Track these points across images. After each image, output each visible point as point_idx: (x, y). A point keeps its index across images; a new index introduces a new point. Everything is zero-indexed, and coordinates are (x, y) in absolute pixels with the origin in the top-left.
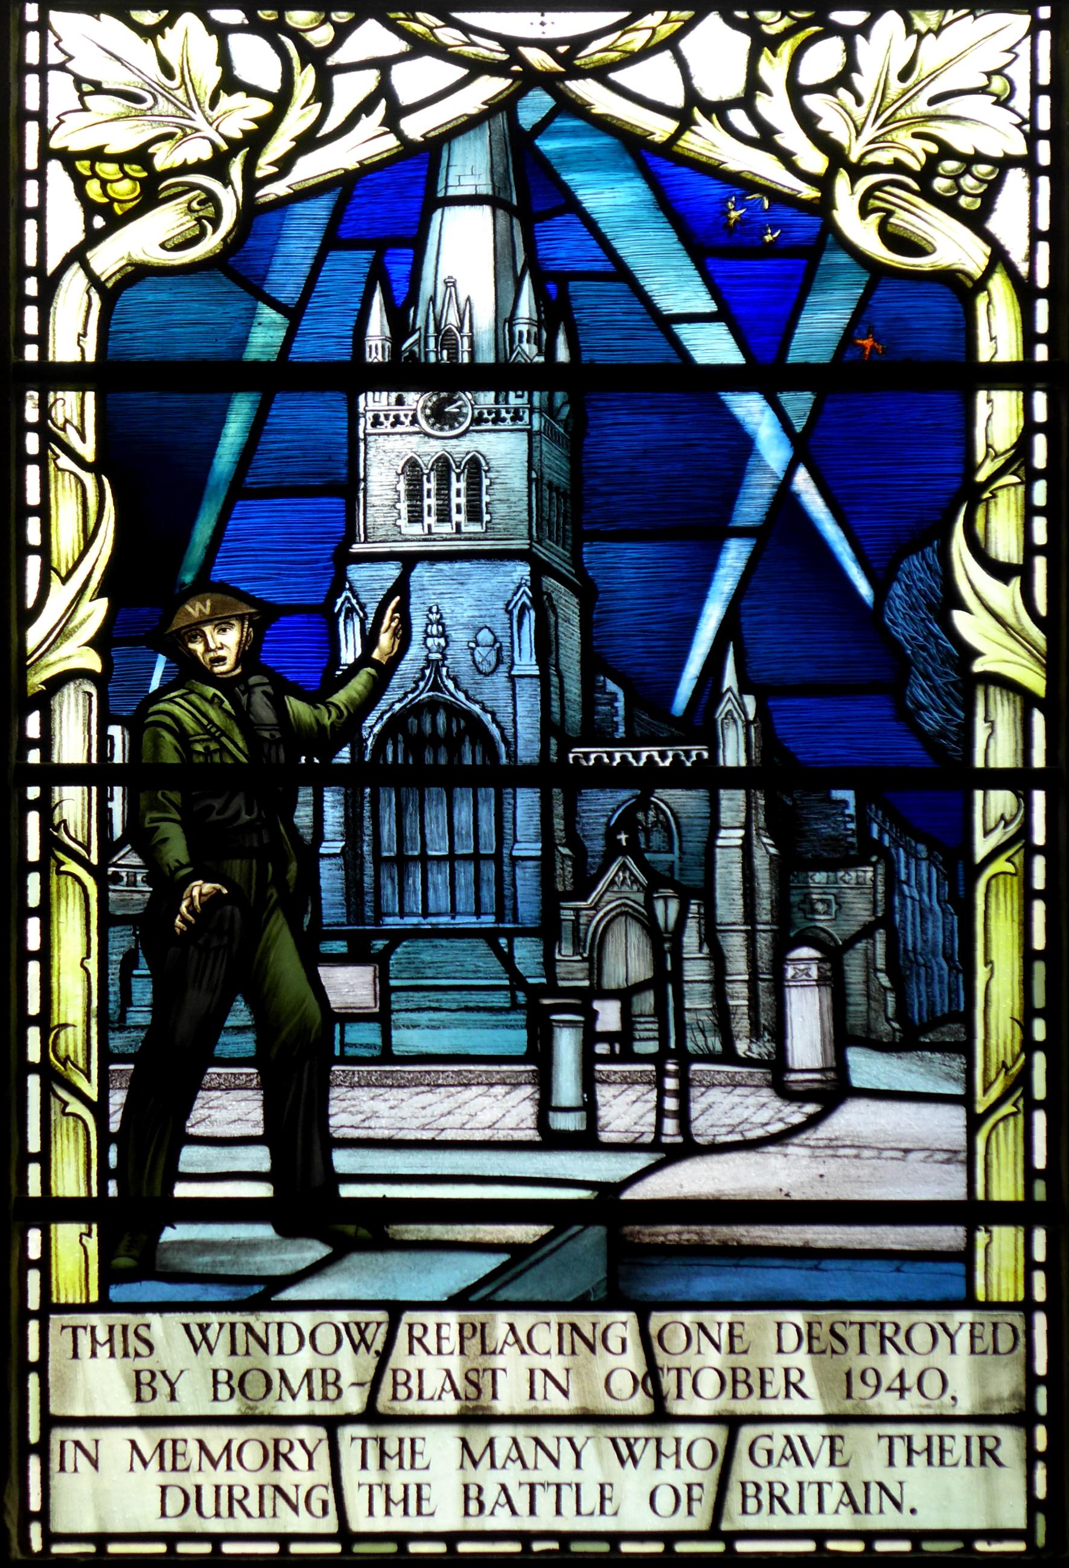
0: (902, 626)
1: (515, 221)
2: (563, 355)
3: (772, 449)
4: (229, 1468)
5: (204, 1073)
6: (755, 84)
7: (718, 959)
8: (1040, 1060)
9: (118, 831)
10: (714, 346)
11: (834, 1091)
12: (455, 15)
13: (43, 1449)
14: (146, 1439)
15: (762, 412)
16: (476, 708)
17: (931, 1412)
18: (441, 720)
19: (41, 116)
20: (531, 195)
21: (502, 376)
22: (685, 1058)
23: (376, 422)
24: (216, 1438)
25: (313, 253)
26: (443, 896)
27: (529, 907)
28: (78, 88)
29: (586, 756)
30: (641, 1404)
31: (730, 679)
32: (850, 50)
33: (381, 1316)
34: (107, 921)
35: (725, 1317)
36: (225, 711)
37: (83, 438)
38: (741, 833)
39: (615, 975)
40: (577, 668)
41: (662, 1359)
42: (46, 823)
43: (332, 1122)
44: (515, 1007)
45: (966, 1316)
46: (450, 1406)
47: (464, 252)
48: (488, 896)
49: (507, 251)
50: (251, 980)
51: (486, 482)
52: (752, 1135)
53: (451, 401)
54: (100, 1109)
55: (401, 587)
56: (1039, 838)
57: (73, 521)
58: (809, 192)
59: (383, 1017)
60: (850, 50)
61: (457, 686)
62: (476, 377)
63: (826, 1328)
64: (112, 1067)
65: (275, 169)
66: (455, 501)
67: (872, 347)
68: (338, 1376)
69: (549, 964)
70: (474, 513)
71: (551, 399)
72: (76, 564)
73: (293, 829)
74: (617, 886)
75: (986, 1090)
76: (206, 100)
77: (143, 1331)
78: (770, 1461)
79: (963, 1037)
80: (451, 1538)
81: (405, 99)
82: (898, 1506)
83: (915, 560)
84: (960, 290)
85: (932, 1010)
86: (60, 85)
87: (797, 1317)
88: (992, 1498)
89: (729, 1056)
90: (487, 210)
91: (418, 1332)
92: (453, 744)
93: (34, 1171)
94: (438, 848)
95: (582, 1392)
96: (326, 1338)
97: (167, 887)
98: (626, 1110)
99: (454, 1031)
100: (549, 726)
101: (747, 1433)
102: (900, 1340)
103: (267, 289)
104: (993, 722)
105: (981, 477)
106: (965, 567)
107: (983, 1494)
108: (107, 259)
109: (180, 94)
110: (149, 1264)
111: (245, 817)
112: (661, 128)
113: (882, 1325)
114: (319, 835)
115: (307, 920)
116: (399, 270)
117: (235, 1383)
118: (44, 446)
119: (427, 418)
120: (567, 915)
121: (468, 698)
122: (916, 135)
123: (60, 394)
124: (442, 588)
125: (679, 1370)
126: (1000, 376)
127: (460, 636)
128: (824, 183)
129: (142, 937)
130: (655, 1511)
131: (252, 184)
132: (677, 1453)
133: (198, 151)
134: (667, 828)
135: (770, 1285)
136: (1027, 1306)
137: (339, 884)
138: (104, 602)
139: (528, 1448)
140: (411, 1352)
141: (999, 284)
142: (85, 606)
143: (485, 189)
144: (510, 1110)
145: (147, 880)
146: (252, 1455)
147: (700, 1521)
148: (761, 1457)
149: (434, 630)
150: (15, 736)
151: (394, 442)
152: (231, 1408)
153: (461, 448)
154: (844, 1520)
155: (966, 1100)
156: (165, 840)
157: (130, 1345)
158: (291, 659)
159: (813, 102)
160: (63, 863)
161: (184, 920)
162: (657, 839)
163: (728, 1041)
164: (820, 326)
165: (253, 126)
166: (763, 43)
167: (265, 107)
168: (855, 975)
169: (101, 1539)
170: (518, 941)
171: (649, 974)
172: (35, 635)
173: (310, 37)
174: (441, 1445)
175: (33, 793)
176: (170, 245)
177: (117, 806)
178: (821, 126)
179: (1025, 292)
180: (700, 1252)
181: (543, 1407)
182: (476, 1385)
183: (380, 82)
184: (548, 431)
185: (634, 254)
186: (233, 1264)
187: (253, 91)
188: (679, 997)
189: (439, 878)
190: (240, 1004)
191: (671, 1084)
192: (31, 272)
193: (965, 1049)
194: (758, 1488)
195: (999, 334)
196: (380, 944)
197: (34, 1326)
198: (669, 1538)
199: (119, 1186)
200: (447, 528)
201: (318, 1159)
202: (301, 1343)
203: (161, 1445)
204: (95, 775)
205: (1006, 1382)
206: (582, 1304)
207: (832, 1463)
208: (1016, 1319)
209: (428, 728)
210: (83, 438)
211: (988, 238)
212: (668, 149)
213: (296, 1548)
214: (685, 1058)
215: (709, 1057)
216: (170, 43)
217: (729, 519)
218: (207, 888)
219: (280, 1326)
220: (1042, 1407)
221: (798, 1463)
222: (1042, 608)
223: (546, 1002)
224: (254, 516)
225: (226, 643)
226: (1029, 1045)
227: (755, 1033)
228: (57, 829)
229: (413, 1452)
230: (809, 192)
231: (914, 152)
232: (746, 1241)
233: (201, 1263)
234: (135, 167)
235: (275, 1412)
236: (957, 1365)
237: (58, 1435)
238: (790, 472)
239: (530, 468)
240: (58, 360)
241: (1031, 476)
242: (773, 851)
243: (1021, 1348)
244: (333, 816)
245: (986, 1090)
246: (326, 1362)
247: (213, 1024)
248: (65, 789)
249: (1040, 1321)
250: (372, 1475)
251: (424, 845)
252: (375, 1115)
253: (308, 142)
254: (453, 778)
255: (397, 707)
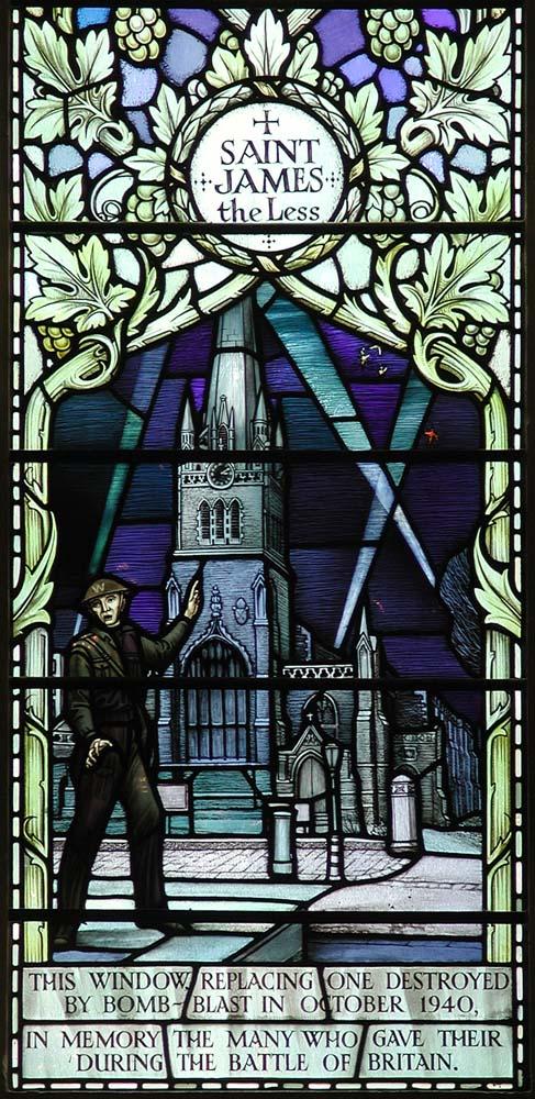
1: (256, 362)
2: (279, 442)
3: (384, 496)
4: (112, 1046)
5: (101, 843)
7: (358, 782)
8: (519, 835)
9: (58, 713)
10: (356, 438)
11: (416, 853)
12: (225, 236)
13: (19, 1036)
14: (70, 1031)
15: (379, 475)
16: (236, 643)
17: (464, 1019)
18: (219, 650)
19: (21, 299)
20: (264, 349)
22: (342, 835)
23: (187, 481)
24: (106, 1031)
25: (155, 381)
26: (219, 751)
28: (40, 283)
29: (292, 670)
30: (319, 1015)
31: (363, 628)
32: (422, 258)
33: (189, 969)
34: (53, 760)
35: (361, 970)
36: (111, 645)
37: (42, 491)
38: (369, 713)
39: (306, 793)
40: (287, 620)
41: (330, 992)
42: (23, 708)
43: (164, 868)
44: (256, 808)
45: (483, 969)
46: (224, 1015)
47: (231, 377)
48: (243, 749)
49: (252, 380)
51: (241, 515)
52: (374, 876)
53: (223, 468)
54: (49, 862)
55: (199, 576)
56: (518, 716)
57: (37, 537)
58: (401, 344)
59: (190, 814)
60: (422, 258)
61: (227, 632)
62: (236, 456)
63: (412, 976)
64: (55, 839)
65: (137, 331)
66: (226, 526)
67: (434, 437)
68: (167, 1000)
69: (273, 785)
70: (235, 534)
71: (273, 467)
72: (39, 563)
73: (145, 711)
74: (307, 744)
75: (492, 852)
76: (102, 289)
77: (70, 977)
78: (384, 1043)
79: (480, 824)
80: (224, 1081)
81: (202, 287)
82: (449, 1066)
83: (455, 559)
84: (474, 404)
85: (465, 810)
86: (30, 278)
87: (397, 970)
88: (495, 1062)
89: (363, 834)
90: (241, 355)
91: (207, 977)
92: (224, 663)
93: (16, 439)
94: (218, 722)
95: (289, 1010)
96: (161, 981)
97: (82, 743)
98: (312, 862)
99: (225, 821)
101: (373, 1029)
102: (449, 982)
103: (132, 403)
104: (495, 652)
105: (488, 512)
106: (482, 567)
107: (494, 1061)
108: (54, 385)
109: (89, 286)
110: (73, 943)
111: (121, 705)
112: (328, 305)
113: (440, 974)
114: (158, 715)
115: (152, 761)
116: (198, 391)
117: (115, 1003)
118: (22, 495)
119: (212, 478)
120: (282, 758)
121: (232, 638)
122: (454, 310)
123: (30, 465)
124: (220, 576)
125: (338, 997)
127: (228, 603)
129: (71, 769)
130: (325, 1065)
131: (126, 340)
132: (337, 1039)
133: (98, 320)
134: (333, 711)
135: (388, 955)
136: (513, 965)
137: (168, 741)
138: (52, 584)
139: (262, 1037)
140: (204, 988)
141: (496, 400)
142: (43, 587)
143: (240, 344)
144: (250, 862)
145: (72, 739)
146: (124, 1040)
147: (349, 1074)
148: (380, 1042)
149: (215, 599)
150: (6, 1067)
151: (196, 490)
152: (114, 1016)
153: (228, 495)
154: (421, 1073)
155: (483, 857)
156: (81, 717)
158: (145, 618)
159: (403, 289)
160: (30, 730)
161: (91, 760)
162: (327, 716)
163: (363, 826)
164: (409, 421)
165: (126, 305)
167: (131, 294)
168: (427, 791)
169: (48, 1082)
170: (257, 772)
171: (324, 791)
172: (18, 603)
173: (153, 250)
174: (219, 1034)
175: (16, 692)
176: (84, 377)
177: (57, 698)
178: (407, 304)
179: (509, 404)
180: (349, 936)
181: (271, 1016)
182: (236, 1005)
183: (189, 279)
184: (272, 484)
185: (315, 382)
186: (115, 942)
187: (126, 284)
188: (339, 803)
189: (218, 737)
190: (118, 806)
191: (334, 849)
192: (16, 393)
193: (482, 830)
194: (378, 1057)
196: (188, 774)
197: (15, 973)
198: (333, 1082)
199: (58, 902)
200: (221, 542)
201: (158, 888)
202: (149, 983)
203: (78, 1034)
204: (45, 683)
205: (502, 1005)
206: (289, 963)
207: (415, 1044)
208: (507, 970)
209: (212, 655)
210: (42, 491)
211: (490, 372)
212: (330, 319)
213: (145, 1086)
214: (342, 835)
215: (353, 835)
217: (363, 536)
218: (103, 742)
219: (138, 974)
220: (521, 1018)
221: (398, 1044)
222: (519, 588)
223: (271, 805)
224: (126, 534)
225: (111, 607)
226: (514, 828)
227: (377, 822)
228: (28, 711)
229: (205, 1039)
230: (401, 344)
232: (372, 931)
233: (99, 942)
234: (68, 330)
235: (136, 1018)
237: (27, 1029)
238: (393, 509)
239: (263, 508)
240: (32, 676)
241: (513, 511)
242: (385, 723)
243: (510, 986)
244: (165, 703)
245: (492, 852)
246: (161, 993)
248: (32, 690)
249: (520, 971)
250: (184, 1050)
251: (210, 720)
252: (186, 865)
253: (153, 315)
254: (225, 684)
255: (197, 642)
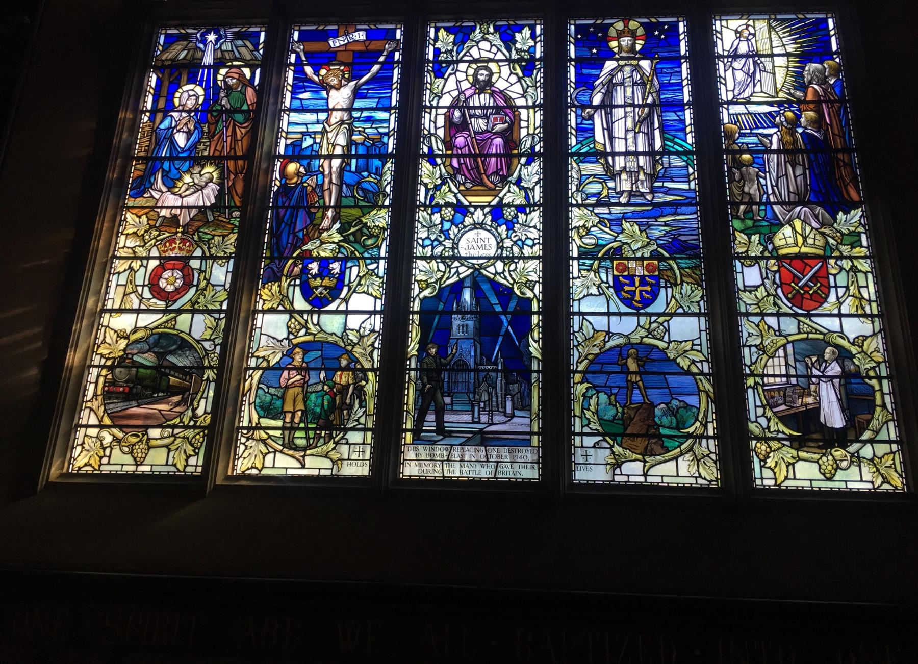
0: (522, 349)
3: (506, 324)
6: (504, 270)
7: (497, 397)
10: (498, 308)
11: (513, 416)
21: (471, 313)
24: (427, 463)
26: (461, 387)
27: (472, 390)
30: (485, 459)
47: (467, 295)
50: (434, 399)
59: (452, 405)
74: (484, 386)
84: (529, 300)
89: (498, 411)
97: (424, 386)
98: (484, 418)
100: (475, 363)
108: (421, 296)
112: (492, 276)
126: (535, 313)
128: (513, 285)
129: (421, 393)
133: (434, 280)
136: (539, 447)
144: (467, 418)
151: (457, 321)
157: (416, 450)
166: (505, 264)
174: (457, 464)
179: (538, 301)
195: (535, 307)
205: (535, 458)
216: (431, 264)
231: (524, 280)
236: (529, 455)
247: (429, 405)
253: (448, 279)
254: (462, 370)
